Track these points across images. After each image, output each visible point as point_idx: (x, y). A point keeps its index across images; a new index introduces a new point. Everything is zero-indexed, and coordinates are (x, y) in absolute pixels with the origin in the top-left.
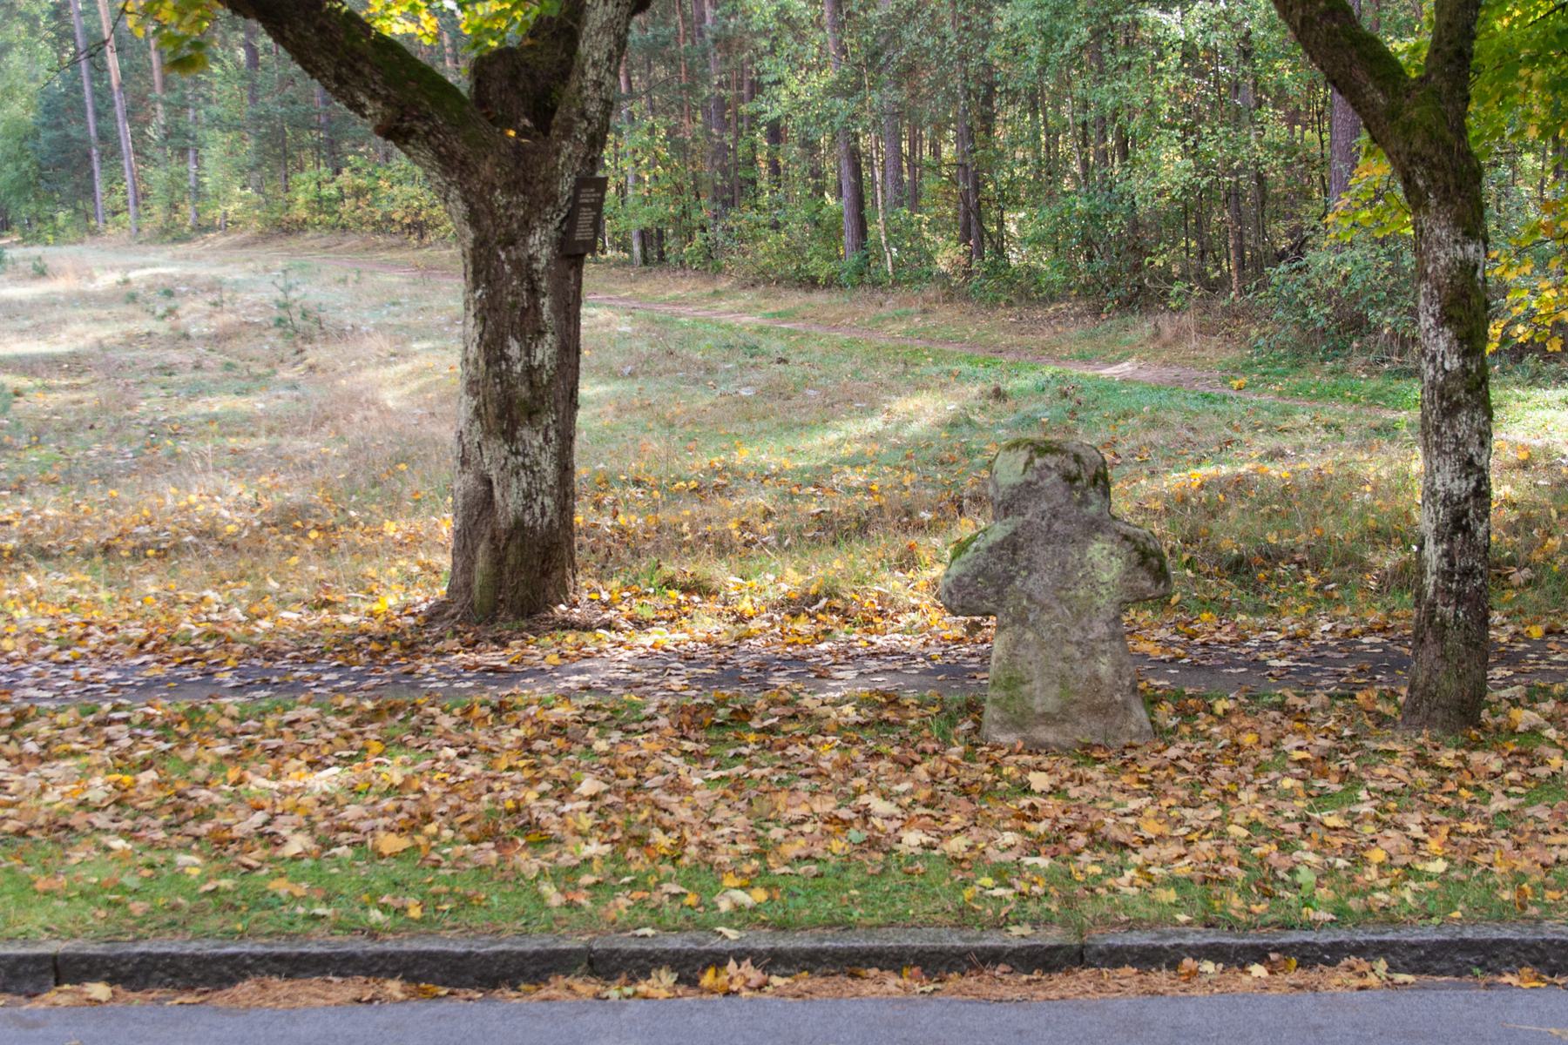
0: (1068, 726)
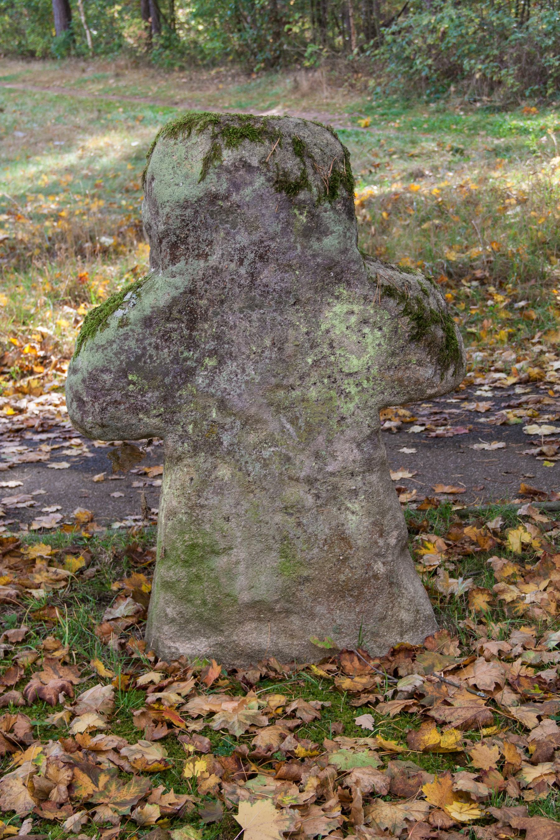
0: (295, 621)
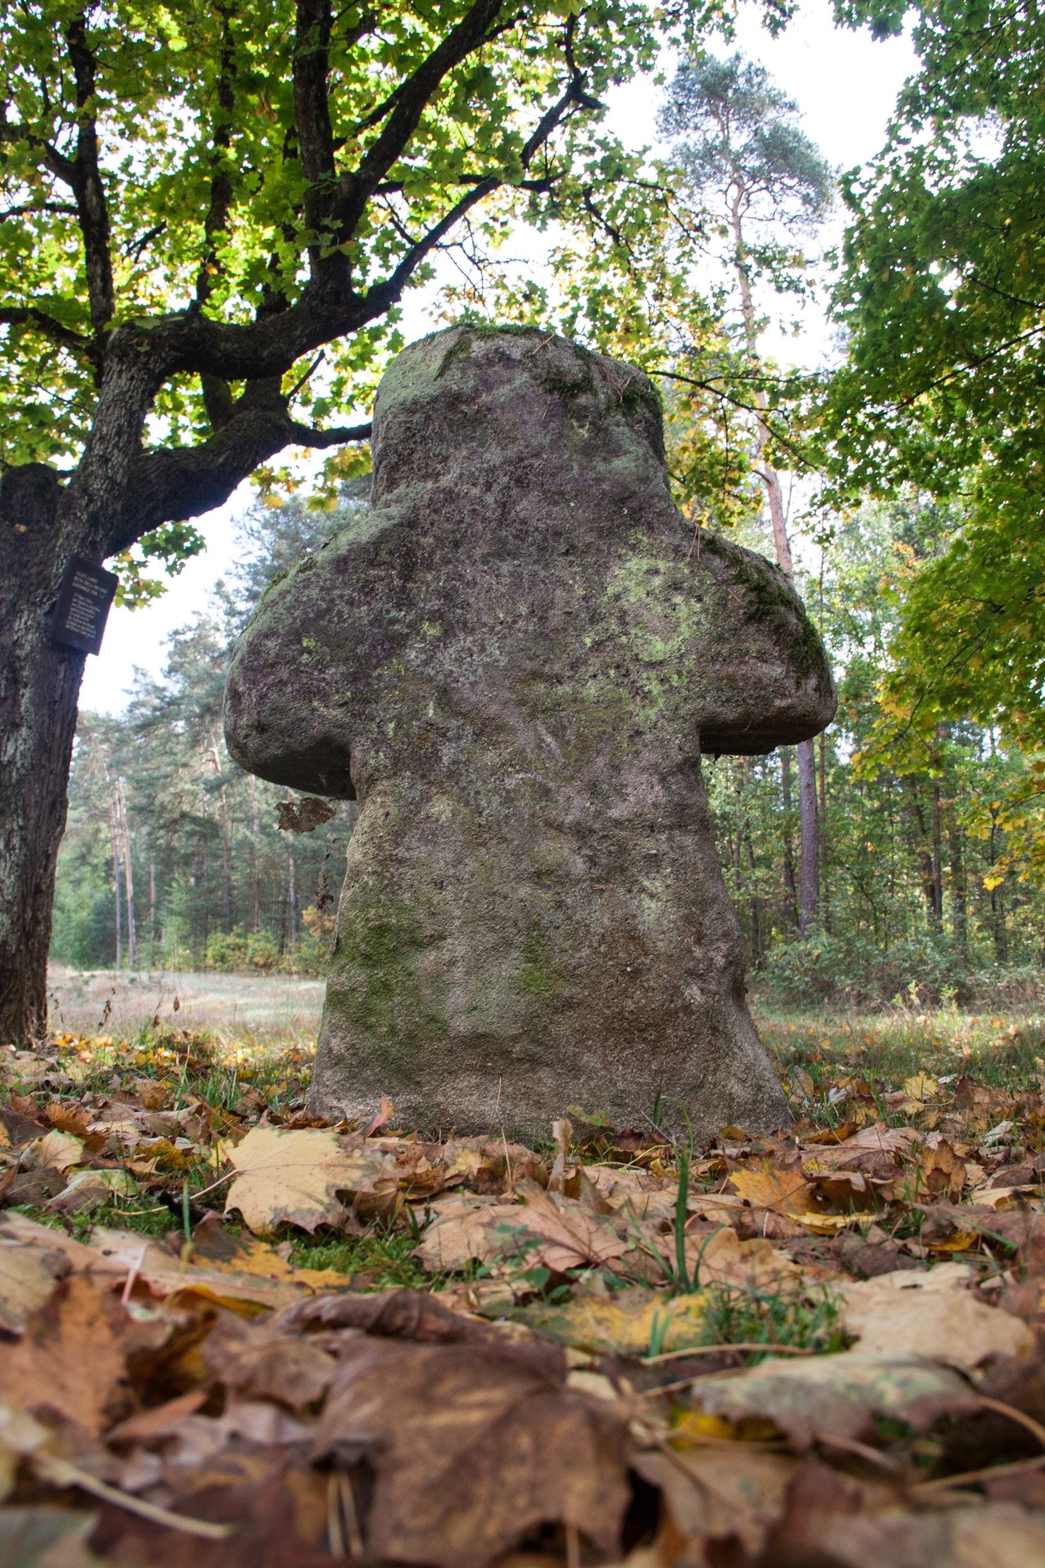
0: (546, 1080)
